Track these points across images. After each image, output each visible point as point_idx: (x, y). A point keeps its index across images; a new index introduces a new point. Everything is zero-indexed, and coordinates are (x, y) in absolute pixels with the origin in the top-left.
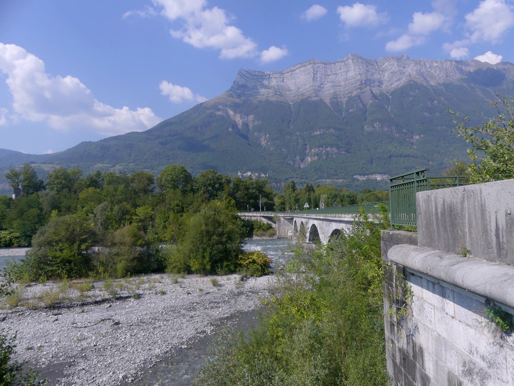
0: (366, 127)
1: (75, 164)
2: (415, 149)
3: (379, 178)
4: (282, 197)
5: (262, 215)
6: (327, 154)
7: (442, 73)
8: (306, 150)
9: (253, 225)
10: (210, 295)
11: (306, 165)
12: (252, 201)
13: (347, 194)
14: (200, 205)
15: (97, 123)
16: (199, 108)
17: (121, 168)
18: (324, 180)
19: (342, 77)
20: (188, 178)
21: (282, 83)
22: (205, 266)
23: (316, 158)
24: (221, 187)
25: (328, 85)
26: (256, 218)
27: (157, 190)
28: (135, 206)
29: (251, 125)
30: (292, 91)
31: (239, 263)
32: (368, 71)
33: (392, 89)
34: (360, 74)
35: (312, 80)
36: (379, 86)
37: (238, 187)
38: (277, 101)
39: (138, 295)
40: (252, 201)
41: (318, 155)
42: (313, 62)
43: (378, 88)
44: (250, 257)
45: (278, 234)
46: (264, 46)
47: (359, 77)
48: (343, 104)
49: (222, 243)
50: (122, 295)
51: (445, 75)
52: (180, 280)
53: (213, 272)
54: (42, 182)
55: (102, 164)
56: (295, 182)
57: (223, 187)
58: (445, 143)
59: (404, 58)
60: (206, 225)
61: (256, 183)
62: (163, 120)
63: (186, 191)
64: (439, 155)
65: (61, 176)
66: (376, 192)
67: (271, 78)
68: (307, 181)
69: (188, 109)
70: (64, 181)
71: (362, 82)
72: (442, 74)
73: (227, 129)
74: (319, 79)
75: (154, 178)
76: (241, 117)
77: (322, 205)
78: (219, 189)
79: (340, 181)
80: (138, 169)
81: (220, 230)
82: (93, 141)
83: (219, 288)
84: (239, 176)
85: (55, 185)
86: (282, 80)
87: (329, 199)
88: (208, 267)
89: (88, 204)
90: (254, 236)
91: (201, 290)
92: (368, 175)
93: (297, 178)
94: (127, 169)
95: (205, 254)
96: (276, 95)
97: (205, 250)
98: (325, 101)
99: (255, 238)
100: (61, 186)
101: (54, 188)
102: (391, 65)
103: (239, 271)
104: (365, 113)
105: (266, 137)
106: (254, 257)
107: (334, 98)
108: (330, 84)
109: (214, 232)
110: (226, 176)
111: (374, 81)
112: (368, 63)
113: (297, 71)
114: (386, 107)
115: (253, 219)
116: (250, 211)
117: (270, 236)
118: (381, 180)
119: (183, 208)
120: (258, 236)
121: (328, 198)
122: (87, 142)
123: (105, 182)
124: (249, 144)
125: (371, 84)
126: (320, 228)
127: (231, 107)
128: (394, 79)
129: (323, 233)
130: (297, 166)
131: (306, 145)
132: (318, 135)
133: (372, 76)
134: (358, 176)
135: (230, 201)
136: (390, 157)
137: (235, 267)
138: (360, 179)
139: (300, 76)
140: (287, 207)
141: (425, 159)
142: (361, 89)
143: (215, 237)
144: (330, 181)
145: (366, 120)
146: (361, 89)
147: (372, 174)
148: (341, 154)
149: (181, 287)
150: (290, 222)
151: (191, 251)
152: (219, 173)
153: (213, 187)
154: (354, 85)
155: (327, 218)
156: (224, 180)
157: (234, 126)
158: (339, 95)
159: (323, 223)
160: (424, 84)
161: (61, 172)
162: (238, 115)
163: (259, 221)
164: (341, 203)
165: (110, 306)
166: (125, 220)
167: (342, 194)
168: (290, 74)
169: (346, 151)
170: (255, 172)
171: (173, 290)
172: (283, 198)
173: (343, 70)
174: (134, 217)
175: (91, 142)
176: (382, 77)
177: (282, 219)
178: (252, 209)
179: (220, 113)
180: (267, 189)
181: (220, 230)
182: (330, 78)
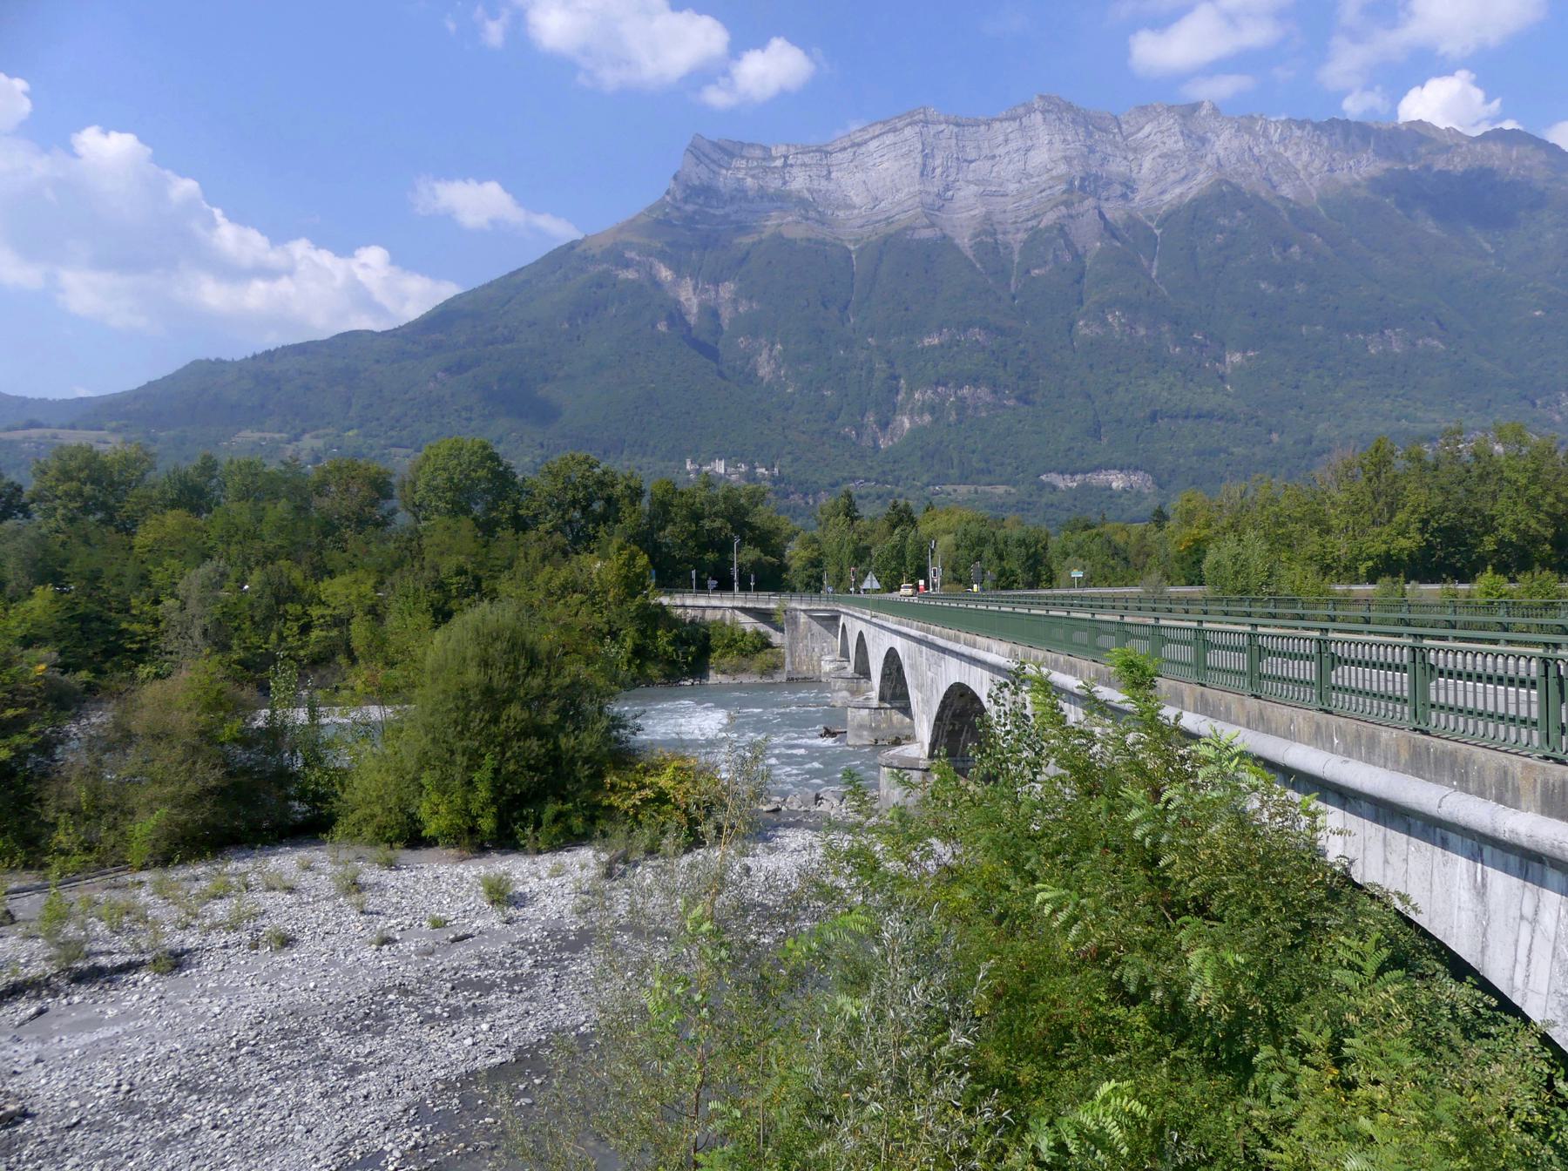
0: (1081, 323)
1: (172, 432)
2: (1228, 396)
3: (1117, 481)
4: (815, 541)
5: (740, 604)
6: (961, 406)
7: (1317, 161)
8: (897, 393)
9: (707, 637)
10: (469, 946)
11: (896, 440)
12: (711, 556)
13: (1017, 533)
14: (536, 570)
15: (212, 294)
16: (564, 258)
17: (319, 444)
18: (949, 488)
19: (1011, 167)
20: (503, 480)
21: (824, 183)
22: (474, 818)
23: (927, 418)
24: (610, 515)
25: (966, 193)
26: (718, 615)
27: (403, 519)
28: (323, 571)
29: (726, 315)
30: (854, 207)
31: (606, 802)
32: (1092, 150)
33: (1164, 208)
34: (1065, 158)
35: (917, 173)
36: (1124, 196)
37: (667, 512)
38: (809, 240)
39: (172, 953)
40: (711, 556)
41: (932, 409)
42: (922, 116)
43: (1121, 202)
44: (648, 780)
45: (788, 667)
46: (746, 38)
47: (1062, 169)
48: (1011, 253)
49: (540, 732)
50: (103, 961)
51: (1326, 168)
52: (370, 874)
53: (505, 841)
54: (19, 489)
55: (259, 430)
56: (854, 493)
57: (618, 510)
58: (1319, 377)
59: (1203, 113)
60: (485, 664)
61: (726, 498)
62: (448, 290)
63: (497, 523)
64: (1302, 413)
65: (80, 470)
66: (1108, 528)
67: (792, 166)
68: (898, 490)
69: (532, 261)
70: (88, 489)
71: (1071, 183)
72: (1317, 163)
73: (654, 326)
74: (938, 171)
75: (393, 480)
76: (695, 289)
77: (936, 572)
78: (604, 518)
79: (1001, 489)
80: (371, 448)
81: (536, 682)
82: (229, 359)
83: (511, 911)
84: (689, 473)
85: (58, 501)
86: (825, 173)
87: (960, 552)
88: (487, 824)
89: (160, 564)
90: (711, 673)
91: (438, 924)
92: (1085, 472)
93: (867, 480)
94: (338, 448)
95: (476, 776)
96: (807, 219)
97: (475, 760)
98: (957, 241)
99: (714, 678)
100: (77, 505)
101: (55, 509)
102: (1162, 132)
103: (604, 834)
104: (1078, 282)
105: (775, 353)
106: (665, 781)
107: (985, 232)
108: (973, 188)
109: (512, 690)
110: (628, 475)
111: (1109, 183)
112: (1087, 122)
113: (873, 145)
114: (1145, 263)
115: (709, 615)
116: (702, 587)
117: (763, 673)
118: (1124, 489)
119: (478, 581)
120: (724, 672)
121: (958, 547)
122: (208, 360)
123: (230, 493)
124: (721, 374)
125: (1100, 190)
126: (912, 666)
127: (663, 256)
128: (1172, 177)
129: (920, 687)
130: (866, 442)
131: (896, 378)
132: (934, 347)
133: (1102, 165)
134: (1054, 475)
135: (633, 557)
136: (1154, 417)
137: (591, 820)
138: (1062, 485)
139: (881, 163)
140: (830, 571)
141: (1257, 424)
142: (1067, 204)
143: (514, 710)
144: (969, 491)
145: (1081, 302)
146: (1067, 204)
147: (1097, 469)
148: (1004, 406)
149: (363, 912)
150: (826, 628)
151: (424, 762)
152: (603, 465)
153: (584, 510)
154: (1048, 192)
155: (930, 637)
156: (620, 488)
157: (676, 316)
158: (999, 223)
159: (921, 652)
160: (1263, 194)
161: (80, 456)
162: (688, 283)
163: (728, 623)
164: (996, 562)
165: (40, 1012)
166: (286, 619)
167: (1000, 534)
168: (849, 154)
169: (1019, 398)
170: (737, 462)
171: (328, 928)
172: (816, 546)
173: (1013, 145)
174: (315, 612)
175: (224, 362)
176: (1135, 169)
177: (803, 618)
178: (712, 583)
179: (630, 275)
180: (761, 517)
181: (536, 682)
182: (974, 171)
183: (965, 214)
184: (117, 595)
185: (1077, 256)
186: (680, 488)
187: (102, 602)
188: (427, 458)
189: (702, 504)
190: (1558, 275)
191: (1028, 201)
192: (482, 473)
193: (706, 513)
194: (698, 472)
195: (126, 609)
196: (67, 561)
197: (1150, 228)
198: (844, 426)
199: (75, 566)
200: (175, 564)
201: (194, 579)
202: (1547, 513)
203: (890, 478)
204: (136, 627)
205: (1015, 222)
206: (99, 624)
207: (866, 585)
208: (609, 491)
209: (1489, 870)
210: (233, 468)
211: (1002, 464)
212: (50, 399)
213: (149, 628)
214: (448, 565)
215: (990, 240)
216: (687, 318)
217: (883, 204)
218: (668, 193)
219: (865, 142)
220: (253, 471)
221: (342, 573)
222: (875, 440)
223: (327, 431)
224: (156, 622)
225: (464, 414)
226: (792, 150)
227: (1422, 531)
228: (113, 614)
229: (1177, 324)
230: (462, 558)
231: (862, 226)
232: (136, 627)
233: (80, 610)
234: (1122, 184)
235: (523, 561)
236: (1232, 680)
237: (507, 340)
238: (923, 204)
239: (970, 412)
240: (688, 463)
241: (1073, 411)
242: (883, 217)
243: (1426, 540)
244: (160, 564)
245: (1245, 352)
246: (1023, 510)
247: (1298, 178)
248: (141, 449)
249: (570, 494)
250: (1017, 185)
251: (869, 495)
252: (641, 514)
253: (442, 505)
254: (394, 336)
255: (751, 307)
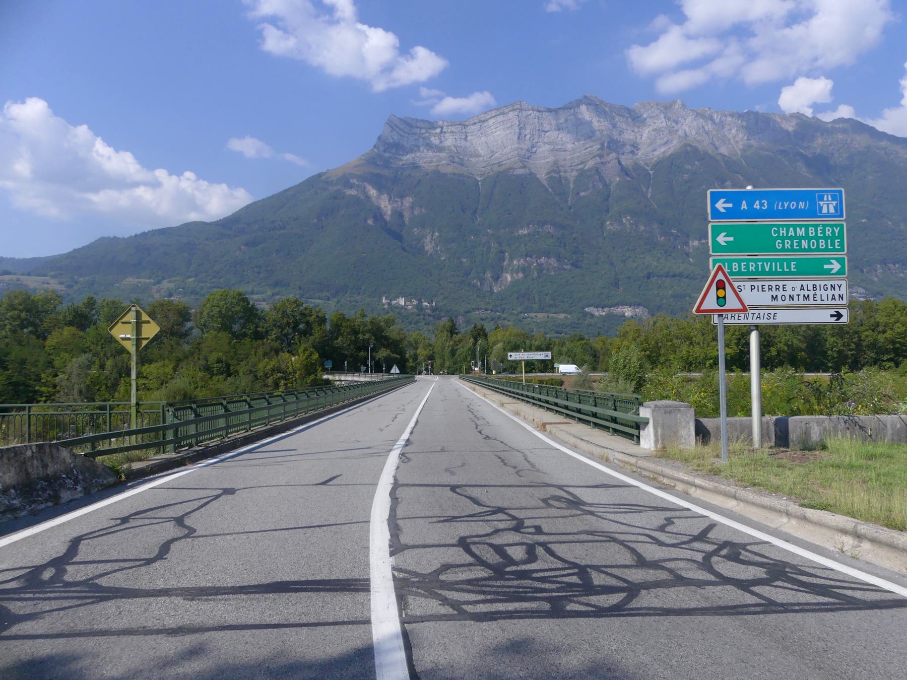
0: (608, 223)
1: (87, 278)
3: (628, 312)
6: (540, 268)
8: (504, 261)
11: (503, 287)
16: (315, 182)
17: (172, 286)
18: (533, 315)
20: (250, 313)
21: (463, 142)
23: (521, 275)
25: (543, 149)
27: (196, 332)
29: (407, 215)
30: (480, 156)
36: (632, 152)
37: (339, 330)
38: (454, 174)
41: (524, 270)
42: (518, 106)
59: (677, 106)
61: (372, 322)
65: (20, 304)
67: (445, 132)
73: (366, 221)
80: (202, 288)
84: (384, 305)
86: (464, 137)
93: (486, 310)
94: (183, 288)
96: (453, 162)
100: (17, 323)
101: (5, 325)
107: (554, 171)
108: (547, 147)
111: (624, 145)
113: (491, 122)
114: (645, 190)
118: (632, 317)
119: (228, 366)
124: (403, 249)
128: (659, 142)
130: (486, 288)
131: (503, 252)
133: (620, 135)
136: (648, 277)
138: (596, 314)
139: (496, 132)
140: (438, 361)
142: (601, 156)
144: (544, 317)
145: (608, 211)
146: (601, 156)
147: (617, 305)
148: (564, 269)
154: (590, 149)
157: (378, 215)
158: (562, 166)
160: (710, 152)
162: (385, 197)
168: (477, 127)
169: (572, 265)
170: (412, 299)
175: (118, 239)
176: (639, 137)
179: (353, 192)
180: (393, 332)
182: (547, 137)
183: (543, 161)
184: (34, 372)
185: (605, 185)
186: (347, 317)
187: (26, 376)
188: (209, 300)
189: (359, 326)
190: (875, 199)
191: (578, 154)
192: (237, 308)
193: (361, 331)
194: (389, 304)
195: (38, 379)
196: (8, 353)
197: (647, 170)
198: (474, 278)
199: (12, 356)
200: (63, 354)
201: (75, 363)
202: (802, 335)
203: (499, 309)
204: (43, 389)
205: (571, 166)
206: (24, 387)
207: (393, 371)
208: (308, 318)
209: (400, 449)
210: (105, 303)
211: (563, 302)
212: (17, 258)
213: (51, 389)
214: (213, 357)
215: (556, 175)
216: (385, 217)
217: (496, 155)
218: (375, 146)
219: (486, 120)
220: (115, 306)
221: (156, 361)
222: (491, 288)
223: (178, 278)
224: (55, 386)
225: (256, 270)
226: (446, 124)
227: (737, 344)
228: (31, 382)
229: (662, 224)
230: (220, 354)
231: (485, 167)
232: (43, 389)
233: (14, 379)
234: (631, 145)
235: (254, 356)
236: (600, 416)
237: (283, 228)
238: (519, 155)
239: (545, 272)
240: (384, 299)
241: (603, 272)
242: (497, 162)
243: (740, 350)
244: (59, 356)
245: (700, 240)
246: (574, 327)
247: (730, 143)
248: (54, 293)
249: (285, 320)
250: (573, 145)
251: (486, 318)
252: (325, 331)
253: (215, 325)
254: (217, 225)
255: (421, 211)
